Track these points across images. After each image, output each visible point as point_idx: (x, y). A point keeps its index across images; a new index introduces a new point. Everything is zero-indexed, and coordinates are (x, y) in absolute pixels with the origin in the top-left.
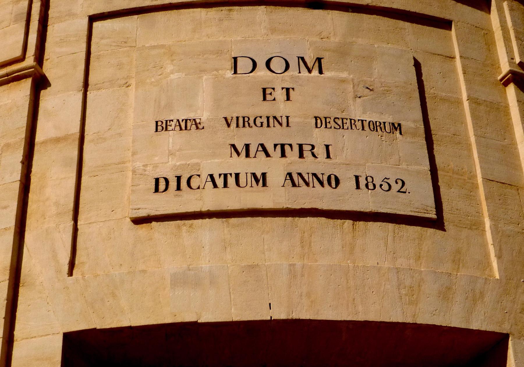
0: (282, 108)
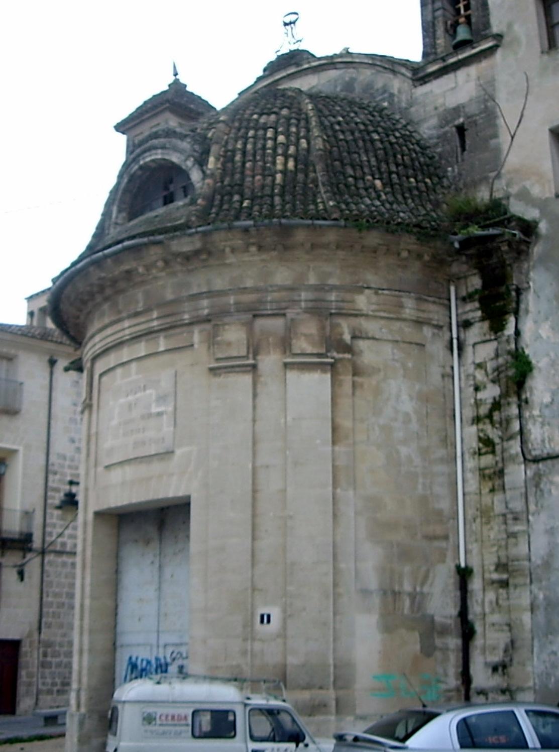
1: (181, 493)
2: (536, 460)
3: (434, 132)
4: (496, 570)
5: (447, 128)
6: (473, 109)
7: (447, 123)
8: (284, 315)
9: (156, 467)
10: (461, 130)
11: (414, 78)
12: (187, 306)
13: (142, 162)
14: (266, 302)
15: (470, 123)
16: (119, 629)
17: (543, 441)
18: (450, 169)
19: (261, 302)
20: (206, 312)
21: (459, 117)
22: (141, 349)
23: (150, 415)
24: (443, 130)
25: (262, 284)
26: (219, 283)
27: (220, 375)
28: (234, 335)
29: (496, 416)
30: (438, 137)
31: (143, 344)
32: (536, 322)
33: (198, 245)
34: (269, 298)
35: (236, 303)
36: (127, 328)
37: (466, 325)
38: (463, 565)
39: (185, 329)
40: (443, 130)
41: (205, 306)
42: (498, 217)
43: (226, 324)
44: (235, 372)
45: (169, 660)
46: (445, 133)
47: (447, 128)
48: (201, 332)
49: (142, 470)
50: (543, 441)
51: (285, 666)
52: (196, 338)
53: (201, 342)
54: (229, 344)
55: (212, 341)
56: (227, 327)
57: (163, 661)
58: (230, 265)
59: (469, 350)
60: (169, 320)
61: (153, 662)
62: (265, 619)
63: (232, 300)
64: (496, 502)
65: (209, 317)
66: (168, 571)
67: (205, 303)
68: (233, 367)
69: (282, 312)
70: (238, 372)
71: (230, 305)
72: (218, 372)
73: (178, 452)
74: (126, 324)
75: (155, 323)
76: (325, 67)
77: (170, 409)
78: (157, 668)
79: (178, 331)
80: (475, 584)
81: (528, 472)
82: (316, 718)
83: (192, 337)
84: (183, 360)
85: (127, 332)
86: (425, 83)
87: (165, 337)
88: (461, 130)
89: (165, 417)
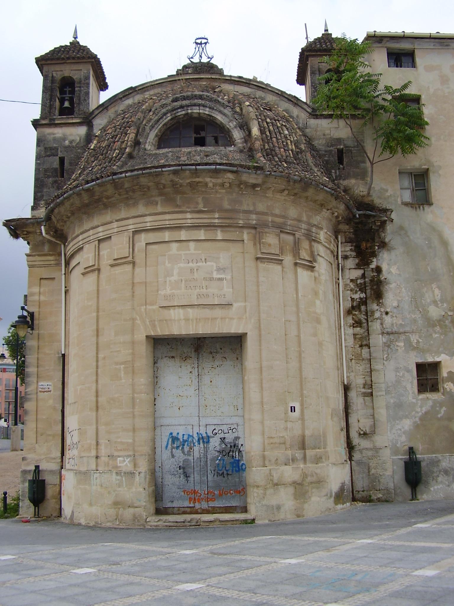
0: (196, 276)
1: (240, 331)
2: (388, 333)
3: (323, 148)
4: (364, 388)
5: (331, 148)
6: (350, 143)
7: (332, 145)
8: (294, 234)
9: (218, 313)
10: (340, 153)
11: (312, 113)
12: (241, 215)
13: (190, 111)
14: (287, 225)
15: (348, 150)
16: (157, 415)
17: (393, 324)
18: (333, 171)
19: (285, 224)
20: (254, 222)
21: (341, 145)
22: (201, 234)
23: (211, 279)
24: (329, 149)
25: (283, 214)
26: (261, 207)
27: (264, 262)
28: (271, 240)
29: (363, 308)
30: (326, 151)
31: (202, 232)
32: (388, 265)
33: (259, 181)
34: (289, 223)
35: (272, 222)
36: (189, 218)
37: (345, 257)
38: (346, 383)
39: (237, 229)
40: (329, 149)
41: (253, 219)
42: (151, 173)
43: (266, 233)
44: (277, 263)
45: (210, 434)
46: (331, 151)
47: (331, 148)
48: (248, 233)
49: (207, 313)
50: (393, 324)
51: (303, 437)
52: (245, 237)
53: (249, 240)
54: (270, 245)
55: (257, 240)
56: (268, 235)
57: (204, 435)
58: (267, 197)
59: (347, 271)
60: (228, 221)
61: (195, 435)
62: (293, 409)
63: (270, 219)
64: (363, 353)
65: (256, 226)
66: (206, 379)
67: (254, 216)
68: (272, 259)
69: (294, 233)
70: (274, 263)
71: (269, 222)
72: (263, 260)
73: (235, 305)
74: (189, 216)
75: (216, 221)
76: (241, 84)
77: (229, 277)
78: (199, 440)
79: (232, 229)
80: (352, 394)
81: (383, 339)
82: (319, 465)
83: (243, 236)
84: (236, 248)
85: (189, 221)
86: (317, 118)
87: (222, 231)
88: (340, 153)
89: (225, 281)
